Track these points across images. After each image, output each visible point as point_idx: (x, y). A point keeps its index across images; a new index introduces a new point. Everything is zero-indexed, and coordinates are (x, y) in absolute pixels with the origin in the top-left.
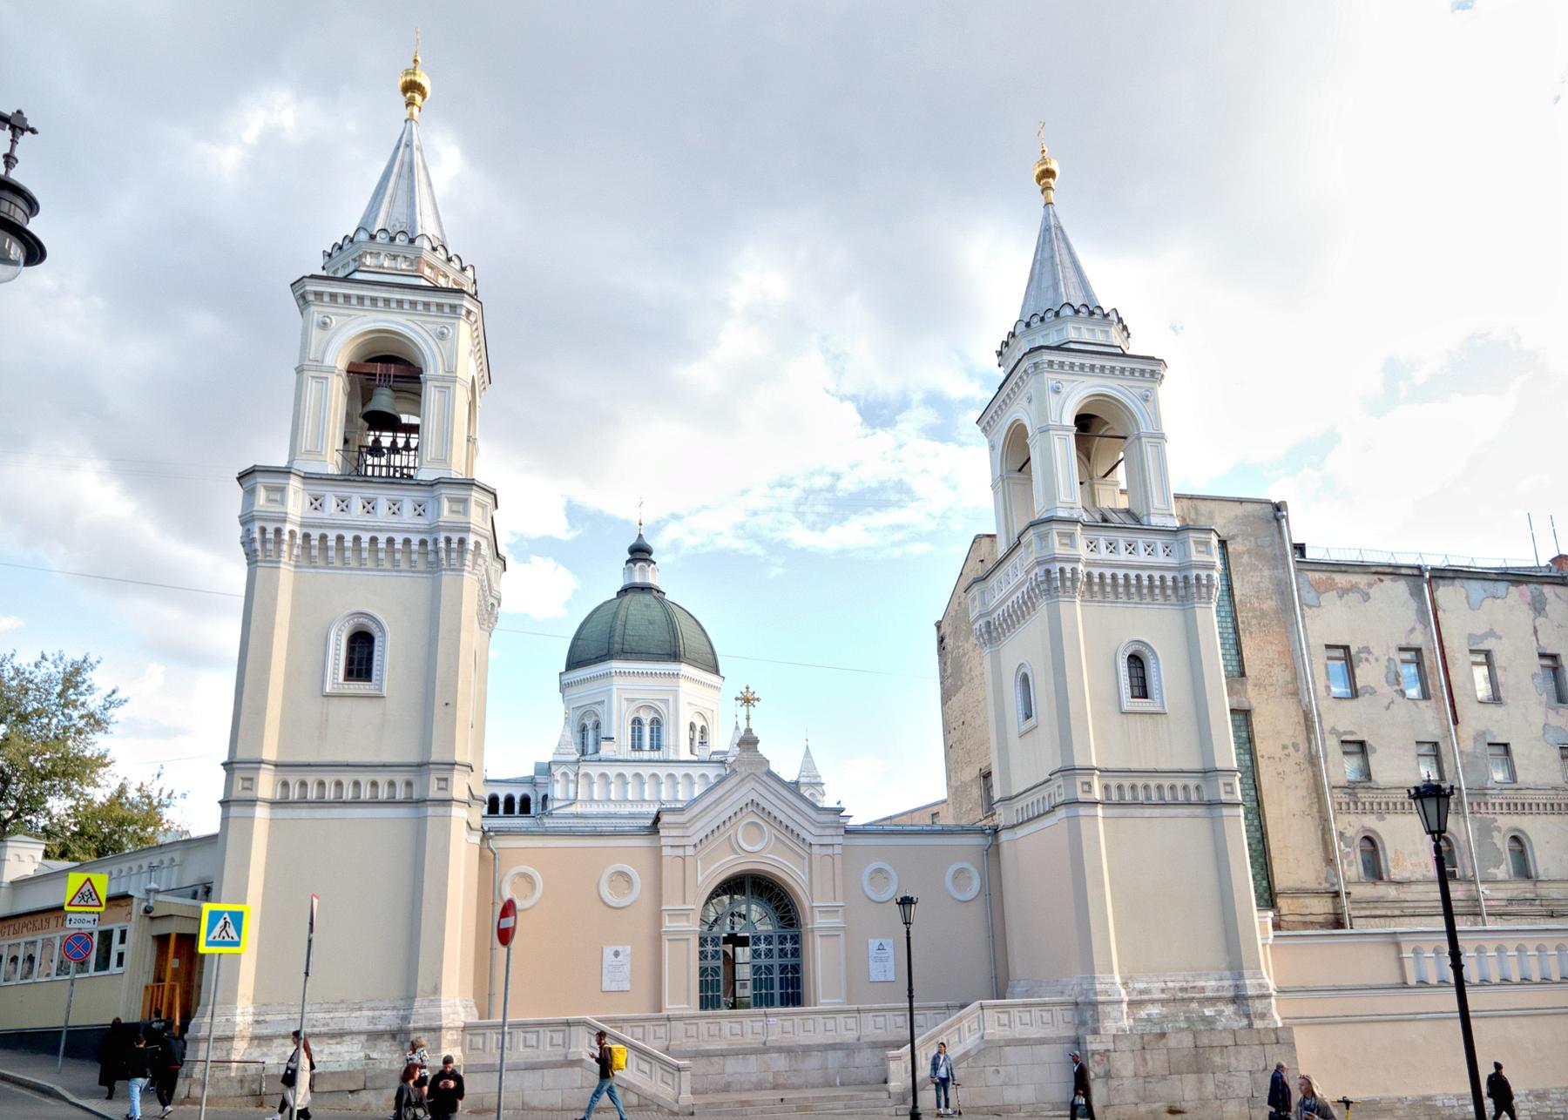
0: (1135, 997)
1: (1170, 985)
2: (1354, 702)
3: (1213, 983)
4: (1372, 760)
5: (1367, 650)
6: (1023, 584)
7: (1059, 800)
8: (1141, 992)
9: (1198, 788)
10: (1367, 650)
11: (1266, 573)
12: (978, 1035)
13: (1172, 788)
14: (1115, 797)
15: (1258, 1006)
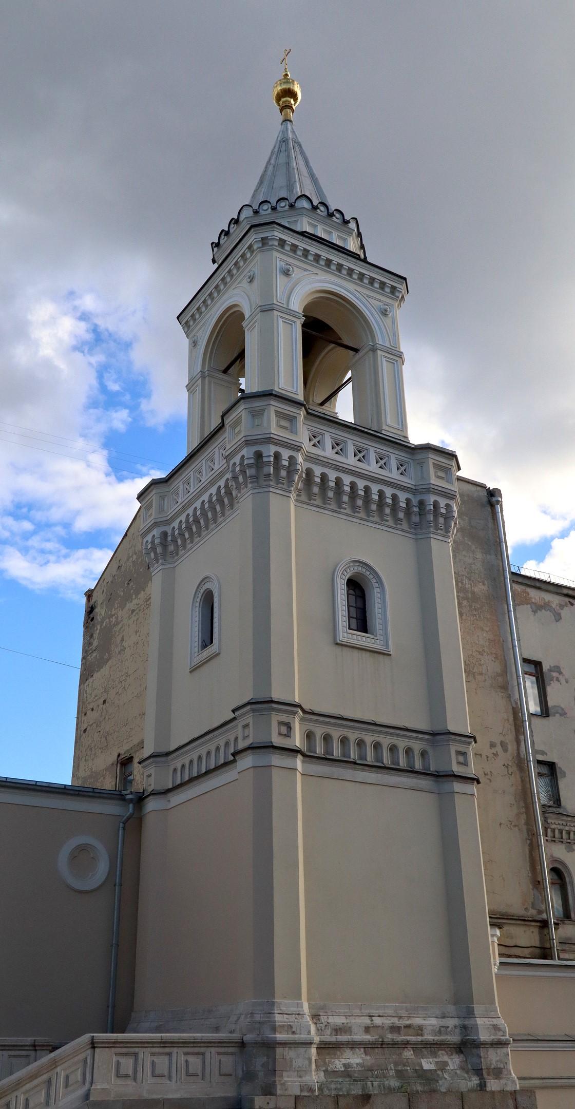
0: (329, 1038)
1: (378, 1021)
2: (544, 721)
3: (433, 1021)
4: (562, 784)
5: (557, 669)
6: (220, 476)
7: (242, 745)
8: (337, 1030)
9: (423, 754)
10: (557, 669)
11: (479, 556)
12: (81, 1091)
13: (393, 749)
14: (320, 750)
15: (492, 1057)
